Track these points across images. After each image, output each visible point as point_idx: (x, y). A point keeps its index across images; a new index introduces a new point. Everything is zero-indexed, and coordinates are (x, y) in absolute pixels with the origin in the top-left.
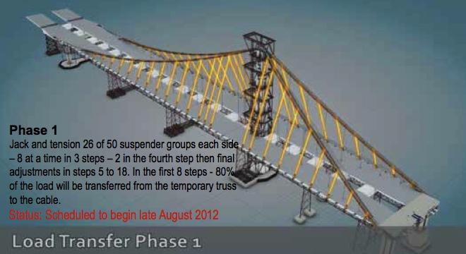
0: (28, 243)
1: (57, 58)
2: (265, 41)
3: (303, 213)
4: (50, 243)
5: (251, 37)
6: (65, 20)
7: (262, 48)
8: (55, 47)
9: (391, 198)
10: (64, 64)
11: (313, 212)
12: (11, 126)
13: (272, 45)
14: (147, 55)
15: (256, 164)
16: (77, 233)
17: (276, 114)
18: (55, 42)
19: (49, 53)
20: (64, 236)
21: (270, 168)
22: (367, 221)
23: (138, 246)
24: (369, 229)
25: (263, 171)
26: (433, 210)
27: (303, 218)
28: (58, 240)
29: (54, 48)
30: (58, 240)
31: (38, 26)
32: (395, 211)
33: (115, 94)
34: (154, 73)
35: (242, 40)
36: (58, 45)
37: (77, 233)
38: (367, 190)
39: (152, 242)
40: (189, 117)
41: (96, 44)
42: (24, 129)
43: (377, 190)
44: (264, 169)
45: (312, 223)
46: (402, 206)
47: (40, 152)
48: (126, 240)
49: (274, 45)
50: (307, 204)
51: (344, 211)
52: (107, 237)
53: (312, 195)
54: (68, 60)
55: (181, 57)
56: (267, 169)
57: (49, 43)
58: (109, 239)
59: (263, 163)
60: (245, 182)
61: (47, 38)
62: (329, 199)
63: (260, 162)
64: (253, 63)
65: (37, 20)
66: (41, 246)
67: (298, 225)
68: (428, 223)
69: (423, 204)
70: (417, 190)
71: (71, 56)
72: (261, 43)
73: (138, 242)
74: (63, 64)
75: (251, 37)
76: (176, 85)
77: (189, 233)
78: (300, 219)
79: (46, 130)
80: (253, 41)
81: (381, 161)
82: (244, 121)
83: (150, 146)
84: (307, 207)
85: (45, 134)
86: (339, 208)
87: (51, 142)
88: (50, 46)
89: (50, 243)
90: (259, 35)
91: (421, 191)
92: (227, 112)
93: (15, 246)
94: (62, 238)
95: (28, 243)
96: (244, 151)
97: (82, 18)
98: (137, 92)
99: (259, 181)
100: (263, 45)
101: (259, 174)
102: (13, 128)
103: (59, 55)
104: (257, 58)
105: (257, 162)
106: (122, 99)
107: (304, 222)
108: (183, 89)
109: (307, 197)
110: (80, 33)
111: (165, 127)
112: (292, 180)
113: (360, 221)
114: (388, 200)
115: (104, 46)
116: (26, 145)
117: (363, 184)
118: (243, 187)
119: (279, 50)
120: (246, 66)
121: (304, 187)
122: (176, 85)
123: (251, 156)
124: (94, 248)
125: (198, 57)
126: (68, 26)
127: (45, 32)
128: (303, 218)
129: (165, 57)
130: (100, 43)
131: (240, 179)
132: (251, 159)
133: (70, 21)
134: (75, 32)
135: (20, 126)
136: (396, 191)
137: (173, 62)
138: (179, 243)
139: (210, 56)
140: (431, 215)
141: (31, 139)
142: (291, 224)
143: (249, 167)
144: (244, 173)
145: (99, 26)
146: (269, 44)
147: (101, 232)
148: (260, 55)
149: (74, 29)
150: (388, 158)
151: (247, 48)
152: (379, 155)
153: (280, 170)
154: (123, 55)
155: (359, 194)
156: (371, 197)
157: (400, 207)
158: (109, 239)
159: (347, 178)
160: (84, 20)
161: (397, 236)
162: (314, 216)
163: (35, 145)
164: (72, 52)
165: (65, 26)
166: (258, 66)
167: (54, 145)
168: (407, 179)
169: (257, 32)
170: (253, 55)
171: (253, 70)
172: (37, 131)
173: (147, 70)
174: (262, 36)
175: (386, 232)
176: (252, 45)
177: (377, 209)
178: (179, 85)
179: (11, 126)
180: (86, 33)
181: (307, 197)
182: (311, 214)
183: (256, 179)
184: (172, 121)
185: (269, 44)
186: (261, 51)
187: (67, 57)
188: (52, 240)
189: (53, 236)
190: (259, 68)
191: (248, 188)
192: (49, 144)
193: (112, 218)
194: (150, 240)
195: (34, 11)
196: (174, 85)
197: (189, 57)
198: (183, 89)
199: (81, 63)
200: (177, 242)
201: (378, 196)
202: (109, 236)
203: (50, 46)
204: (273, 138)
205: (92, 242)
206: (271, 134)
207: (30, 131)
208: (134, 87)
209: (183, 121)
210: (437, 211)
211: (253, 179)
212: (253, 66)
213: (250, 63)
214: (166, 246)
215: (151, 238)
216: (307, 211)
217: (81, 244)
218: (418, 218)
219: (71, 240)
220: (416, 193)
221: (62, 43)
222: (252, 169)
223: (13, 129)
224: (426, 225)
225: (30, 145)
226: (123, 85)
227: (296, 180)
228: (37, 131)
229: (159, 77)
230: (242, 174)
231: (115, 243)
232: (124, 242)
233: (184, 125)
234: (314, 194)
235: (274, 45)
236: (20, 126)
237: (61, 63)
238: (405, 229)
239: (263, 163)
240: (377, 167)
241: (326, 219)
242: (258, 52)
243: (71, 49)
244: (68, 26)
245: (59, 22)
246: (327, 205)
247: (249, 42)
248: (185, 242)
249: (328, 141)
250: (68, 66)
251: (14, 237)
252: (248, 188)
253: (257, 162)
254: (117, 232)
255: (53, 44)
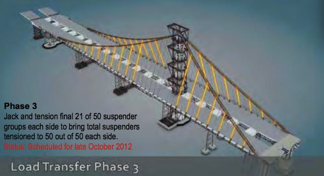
0: (21, 168)
1: (42, 41)
2: (182, 29)
3: (207, 147)
4: (36, 168)
5: (173, 27)
6: (47, 15)
7: (180, 34)
8: (39, 34)
9: (268, 137)
10: (46, 45)
11: (214, 146)
12: (5, 103)
13: (187, 32)
14: (107, 42)
15: (176, 114)
16: (54, 161)
17: (207, 89)
18: (40, 30)
19: (36, 38)
20: (46, 163)
21: (186, 116)
22: (251, 153)
23: (96, 170)
24: (251, 159)
25: (180, 118)
26: (295, 145)
27: (208, 151)
28: (42, 166)
29: (39, 34)
30: (42, 166)
31: (28, 19)
32: (270, 146)
33: (81, 65)
34: (116, 57)
35: (166, 29)
36: (42, 33)
37: (54, 161)
38: (251, 132)
39: (106, 167)
40: (131, 81)
41: (68, 31)
42: (14, 105)
43: (258, 132)
44: (181, 117)
45: (214, 154)
46: (275, 142)
47: (27, 122)
48: (88, 166)
49: (188, 33)
50: (210, 141)
51: (229, 142)
52: (75, 164)
53: (214, 135)
54: (50, 42)
55: (136, 42)
56: (184, 117)
57: (36, 30)
58: (76, 165)
59: (181, 113)
60: (169, 126)
61: (35, 28)
62: (225, 138)
63: (178, 112)
64: (173, 45)
65: (27, 15)
66: (30, 170)
67: (204, 156)
68: (293, 154)
69: (289, 141)
70: (285, 132)
71: (50, 40)
72: (179, 31)
73: (96, 167)
74: (45, 45)
75: (173, 27)
76: (132, 65)
77: (131, 161)
78: (206, 151)
79: (29, 106)
80: (174, 29)
81: (255, 106)
82: (168, 85)
83: (126, 128)
84: (210, 143)
85: (28, 108)
86: (232, 144)
87: (36, 115)
88: (36, 33)
89: (36, 168)
90: (178, 26)
91: (288, 132)
92: (156, 78)
93: (13, 170)
94: (44, 164)
95: (21, 168)
96: (167, 105)
97: (58, 14)
98: (96, 65)
99: (178, 125)
100: (181, 32)
101: (178, 120)
102: (7, 105)
103: (43, 39)
104: (177, 41)
105: (176, 112)
106: (85, 69)
107: (209, 153)
108: (127, 62)
109: (211, 136)
110: (56, 24)
111: (114, 88)
112: (235, 146)
113: (246, 153)
114: (265, 139)
115: (81, 37)
116: (16, 117)
117: (248, 128)
118: (167, 130)
119: (191, 36)
120: (169, 47)
121: (163, 103)
122: (132, 65)
123: (173, 108)
124: (66, 171)
125: (148, 40)
126: (49, 19)
127: (33, 24)
128: (208, 151)
129: (122, 42)
130: (71, 31)
131: (166, 124)
132: (173, 110)
133: (50, 16)
134: (53, 24)
135: (11, 103)
136: (270, 131)
137: (130, 45)
138: (124, 168)
139: (151, 40)
140: (295, 148)
141: (20, 112)
142: (201, 155)
143: (171, 116)
144: (168, 120)
145: (69, 19)
146: (185, 32)
147: (71, 160)
148: (179, 39)
149: (53, 22)
150: (271, 114)
151: (170, 35)
152: (265, 113)
153: (192, 118)
154: (102, 49)
155: (245, 134)
156: (253, 137)
157: (273, 143)
158: (76, 165)
159: (229, 121)
160: (59, 15)
161: (271, 163)
162: (215, 149)
163: (23, 117)
164: (52, 36)
165: (46, 19)
166: (177, 47)
167: (38, 117)
168: (273, 119)
169: (176, 23)
170: (174, 39)
171: (174, 50)
172: (22, 107)
173: (111, 54)
174: (180, 27)
175: (265, 161)
176: (173, 32)
177: (258, 145)
178: (134, 65)
179: (5, 103)
180: (61, 24)
181: (211, 136)
182: (213, 148)
183: (176, 124)
184: (119, 84)
185: (185, 32)
186: (179, 36)
187: (47, 40)
188: (38, 165)
189: (38, 163)
190: (178, 48)
191: (171, 130)
192: (34, 116)
193: (70, 129)
194: (104, 166)
195: (25, 10)
196: (130, 65)
197: (142, 41)
198: (127, 62)
199: (57, 45)
200: (122, 167)
201: (258, 135)
202: (76, 164)
203: (36, 33)
204: (187, 96)
205: (65, 167)
206: (187, 93)
207: (17, 107)
208: (93, 61)
209: (126, 84)
210: (298, 146)
211: (174, 124)
212: (174, 46)
213: (172, 44)
214: (115, 170)
215: (105, 164)
216: (210, 146)
217: (57, 169)
218: (286, 151)
219: (51, 166)
220: (284, 133)
221: (44, 31)
222: (173, 117)
223: (6, 105)
224: (291, 155)
225: (19, 117)
226: (87, 60)
227: (197, 121)
228: (22, 107)
229: (119, 60)
230: (166, 121)
231: (81, 167)
232: (86, 166)
233: (127, 87)
234: (215, 134)
235: (188, 33)
236: (11, 103)
237: (44, 44)
238: (277, 158)
239: (181, 113)
240: (263, 119)
241: (222, 151)
242: (177, 37)
243: (50, 35)
244: (49, 19)
245: (43, 17)
246: (223, 142)
247: (171, 30)
248: (128, 167)
249: (219, 96)
250: (49, 46)
251: (12, 164)
252: (171, 130)
253: (176, 112)
254: (83, 160)
255: (39, 31)
